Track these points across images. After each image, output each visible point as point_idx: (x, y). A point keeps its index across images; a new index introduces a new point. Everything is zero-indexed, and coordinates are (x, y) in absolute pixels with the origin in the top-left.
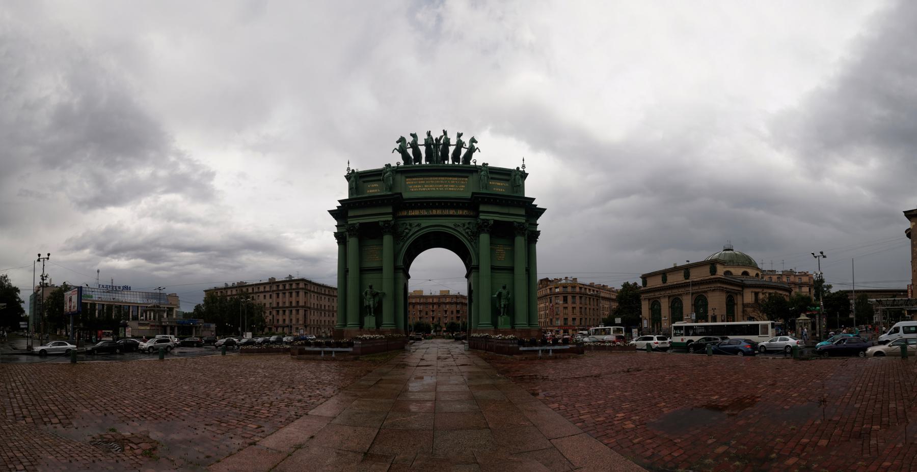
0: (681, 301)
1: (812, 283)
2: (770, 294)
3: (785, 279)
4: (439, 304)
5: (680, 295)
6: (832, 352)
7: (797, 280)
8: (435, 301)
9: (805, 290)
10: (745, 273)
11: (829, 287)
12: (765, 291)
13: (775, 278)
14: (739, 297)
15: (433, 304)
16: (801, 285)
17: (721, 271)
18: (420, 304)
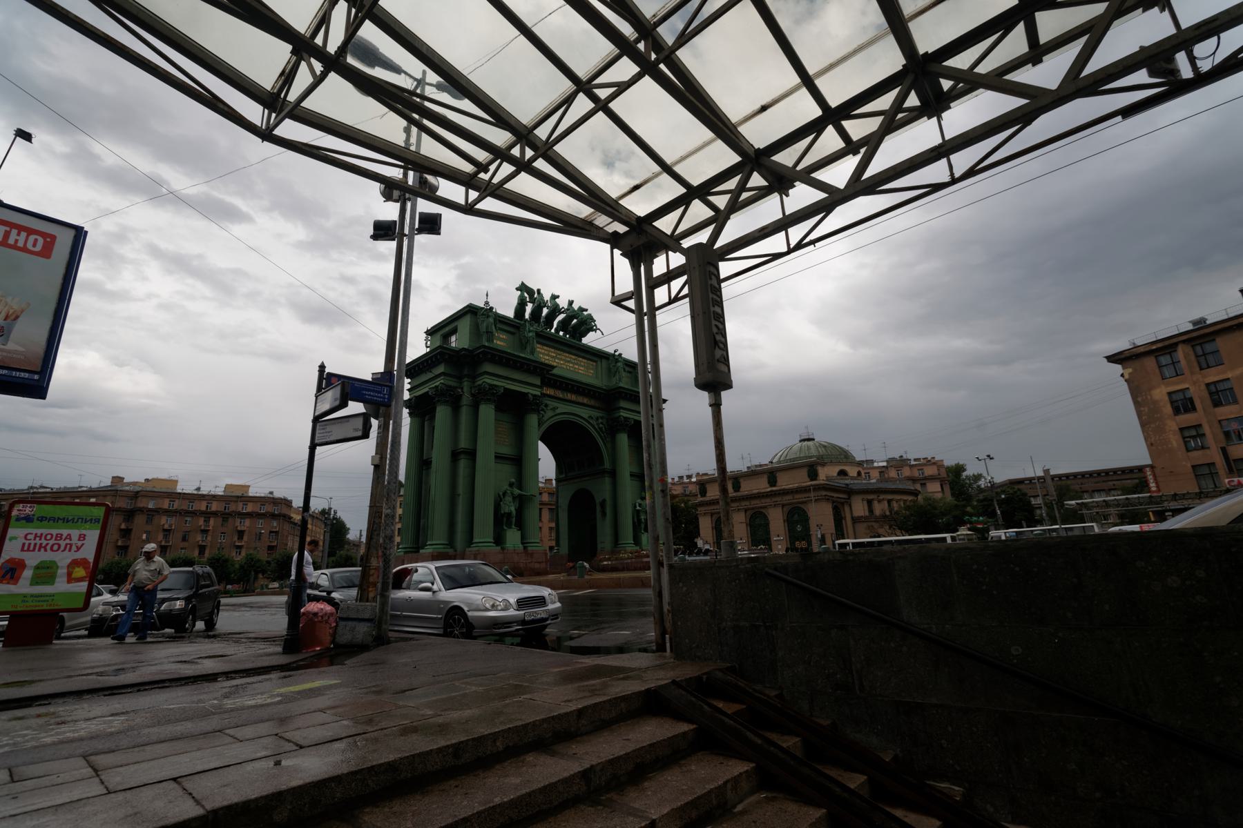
0: (765, 517)
1: (944, 474)
2: (905, 501)
3: (893, 473)
4: (225, 516)
5: (765, 507)
6: (971, 173)
7: (916, 474)
8: (215, 507)
9: (934, 488)
10: (843, 473)
11: (978, 477)
12: (881, 497)
13: (875, 475)
14: (847, 509)
15: (207, 515)
16: (924, 481)
17: (825, 473)
18: (167, 512)
